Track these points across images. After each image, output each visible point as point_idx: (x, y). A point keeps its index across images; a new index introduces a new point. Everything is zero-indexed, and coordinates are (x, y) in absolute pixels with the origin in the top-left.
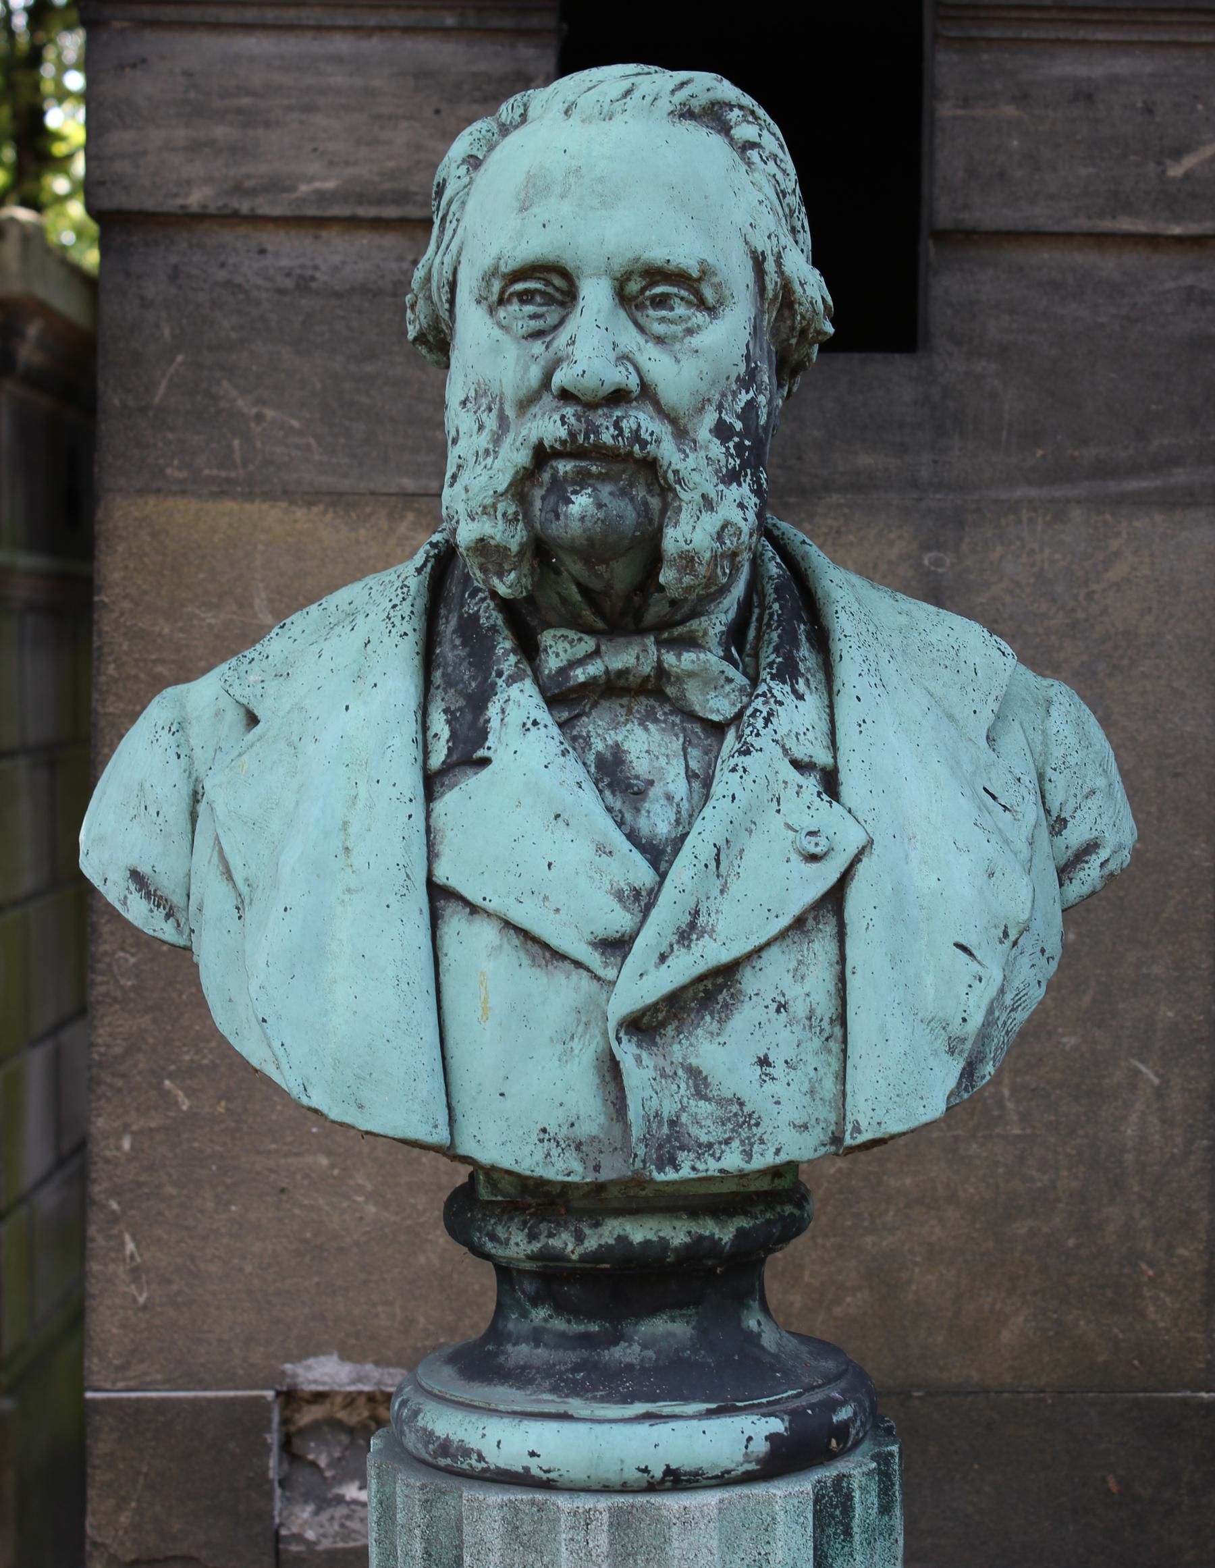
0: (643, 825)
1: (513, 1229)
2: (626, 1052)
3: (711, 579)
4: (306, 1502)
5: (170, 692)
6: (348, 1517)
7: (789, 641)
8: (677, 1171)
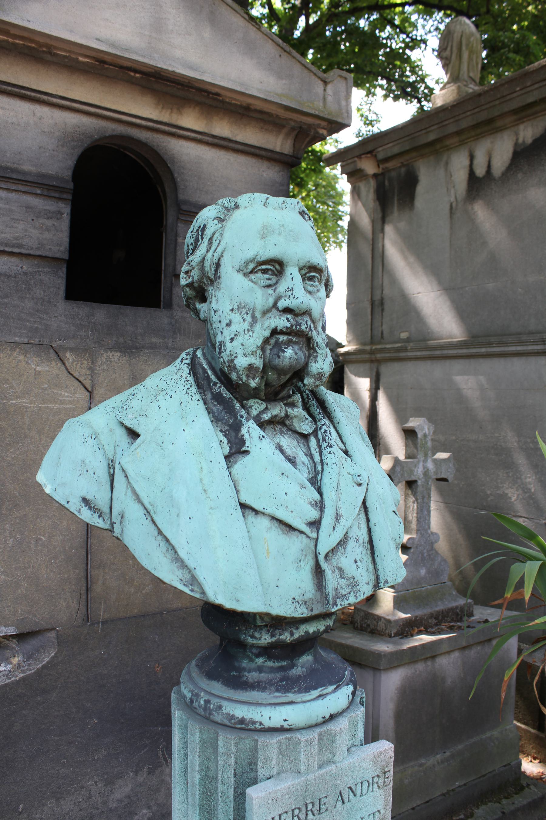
1: (263, 633)
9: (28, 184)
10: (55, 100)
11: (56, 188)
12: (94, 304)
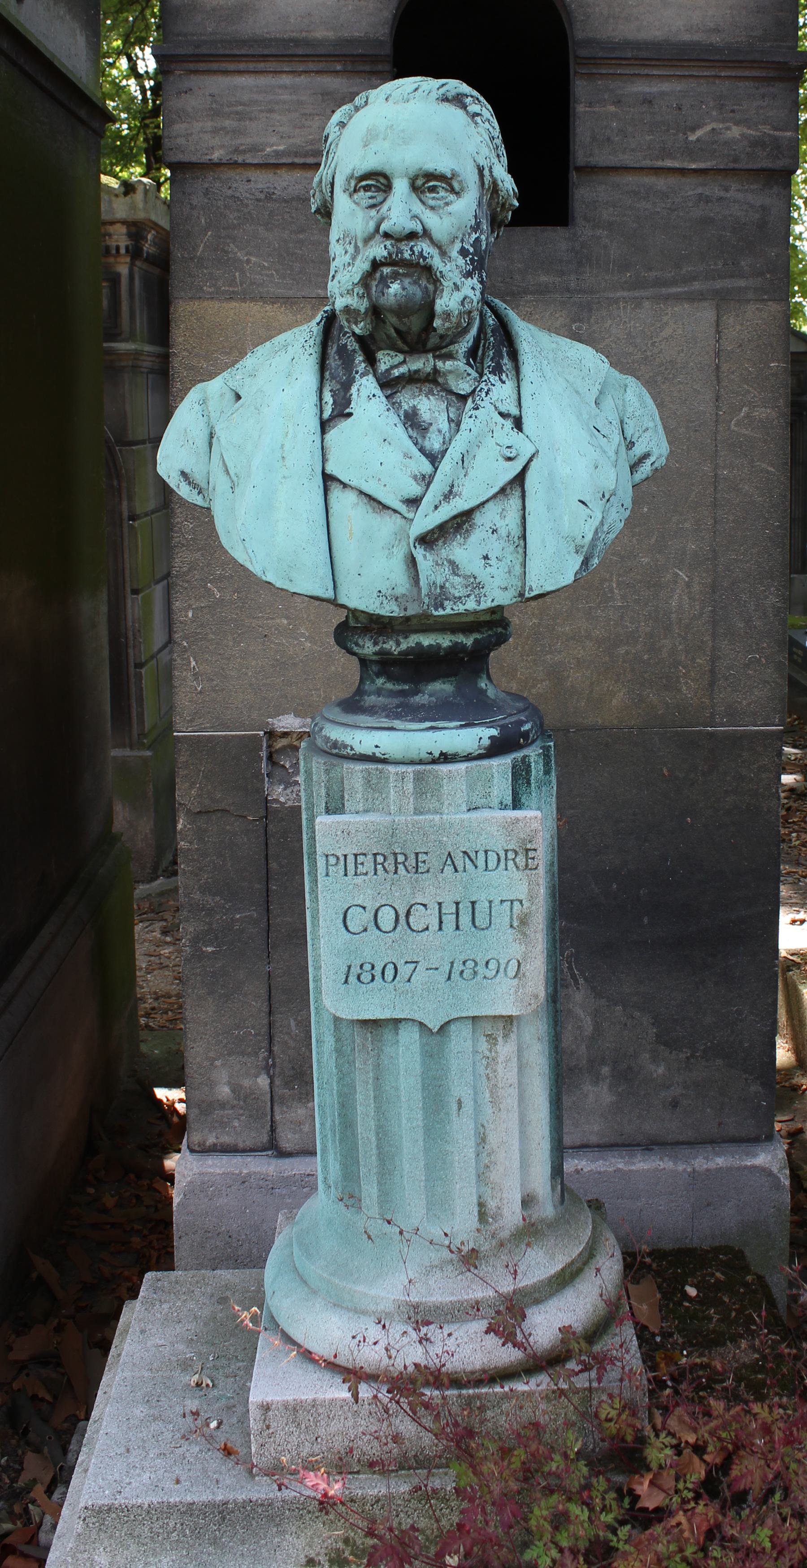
0: (427, 444)
1: (366, 640)
2: (419, 553)
3: (459, 324)
5: (200, 386)
7: (498, 355)
9: (322, 59)
11: (373, 59)
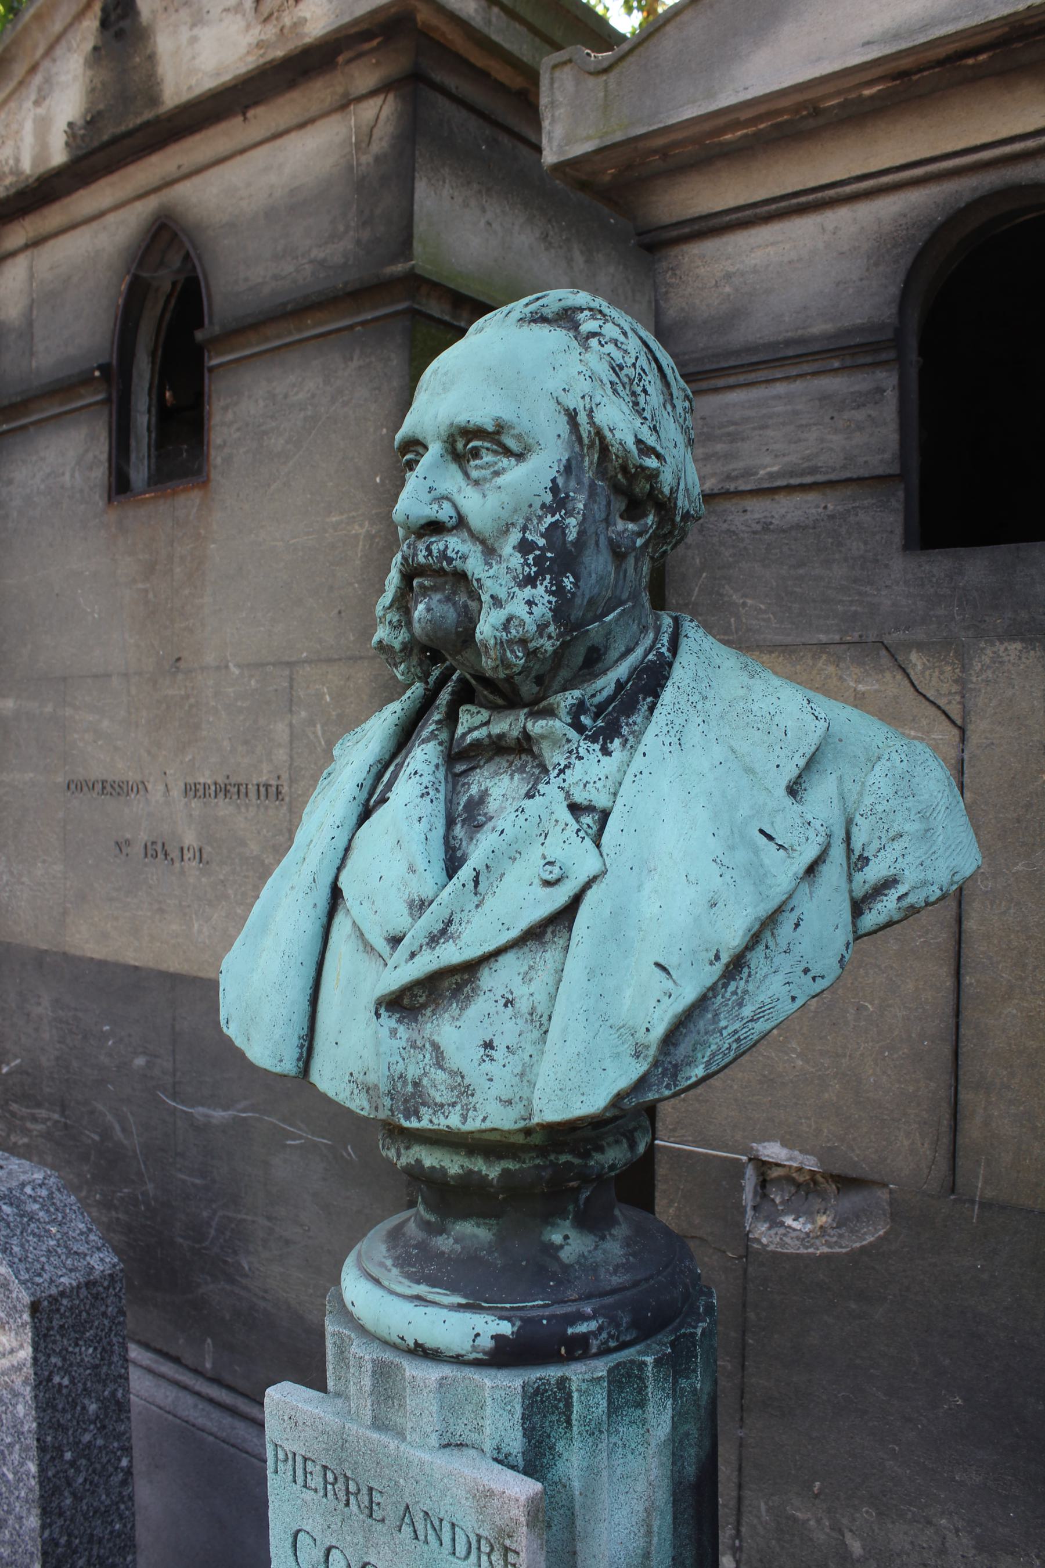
4: (765, 1221)
6: (785, 1235)
8: (420, 1121)
9: (817, 357)
10: (848, 189)
12: (962, 551)
